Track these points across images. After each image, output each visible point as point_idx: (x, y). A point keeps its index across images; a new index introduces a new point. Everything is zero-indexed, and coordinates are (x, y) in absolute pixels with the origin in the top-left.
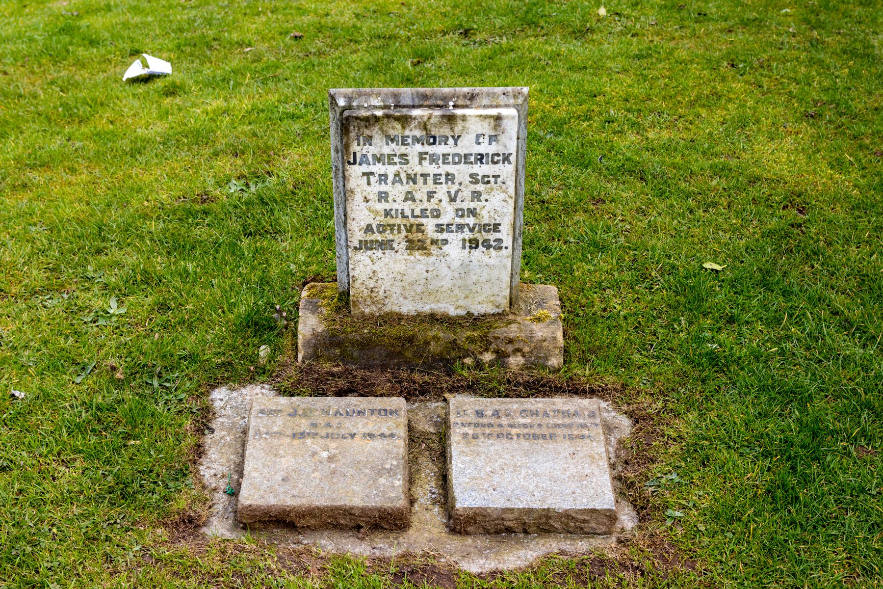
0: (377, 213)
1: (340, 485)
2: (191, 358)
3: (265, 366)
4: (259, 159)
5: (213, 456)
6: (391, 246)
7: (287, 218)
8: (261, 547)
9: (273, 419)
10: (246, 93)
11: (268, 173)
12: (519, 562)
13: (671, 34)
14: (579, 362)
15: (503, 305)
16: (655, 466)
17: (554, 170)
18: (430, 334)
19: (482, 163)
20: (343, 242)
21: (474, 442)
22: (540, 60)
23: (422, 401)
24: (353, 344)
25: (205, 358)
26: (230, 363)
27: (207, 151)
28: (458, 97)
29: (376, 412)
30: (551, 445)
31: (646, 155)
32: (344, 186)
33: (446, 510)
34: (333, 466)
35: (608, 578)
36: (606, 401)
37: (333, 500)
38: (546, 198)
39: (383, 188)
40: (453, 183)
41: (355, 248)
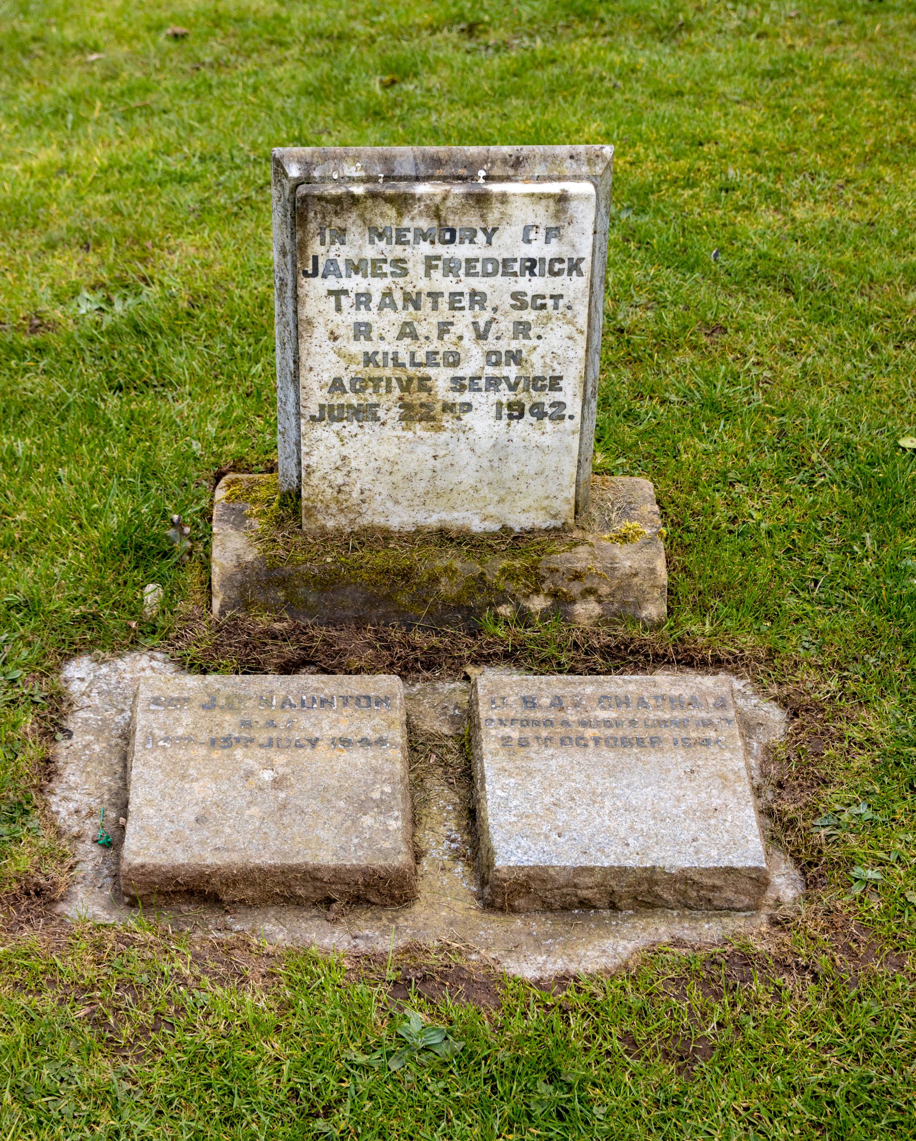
0: (351, 358)
1: (295, 829)
2: (29, 607)
3: (155, 620)
4: (128, 255)
5: (72, 778)
6: (375, 414)
7: (182, 360)
8: (163, 937)
9: (176, 714)
10: (97, 136)
11: (144, 279)
12: (604, 960)
13: (824, 34)
14: (693, 611)
15: (563, 515)
16: (829, 791)
17: (637, 275)
18: (439, 564)
19: (532, 274)
20: (291, 408)
21: (522, 752)
22: (602, 79)
23: (427, 680)
24: (307, 581)
25: (52, 608)
26: (95, 617)
27: (35, 241)
28: (493, 162)
29: (352, 702)
30: (653, 757)
31: (794, 249)
32: (296, 312)
33: (476, 870)
34: (282, 795)
35: (757, 986)
36: (742, 678)
37: (285, 855)
38: (627, 324)
39: (363, 316)
40: (483, 308)
41: (313, 418)
